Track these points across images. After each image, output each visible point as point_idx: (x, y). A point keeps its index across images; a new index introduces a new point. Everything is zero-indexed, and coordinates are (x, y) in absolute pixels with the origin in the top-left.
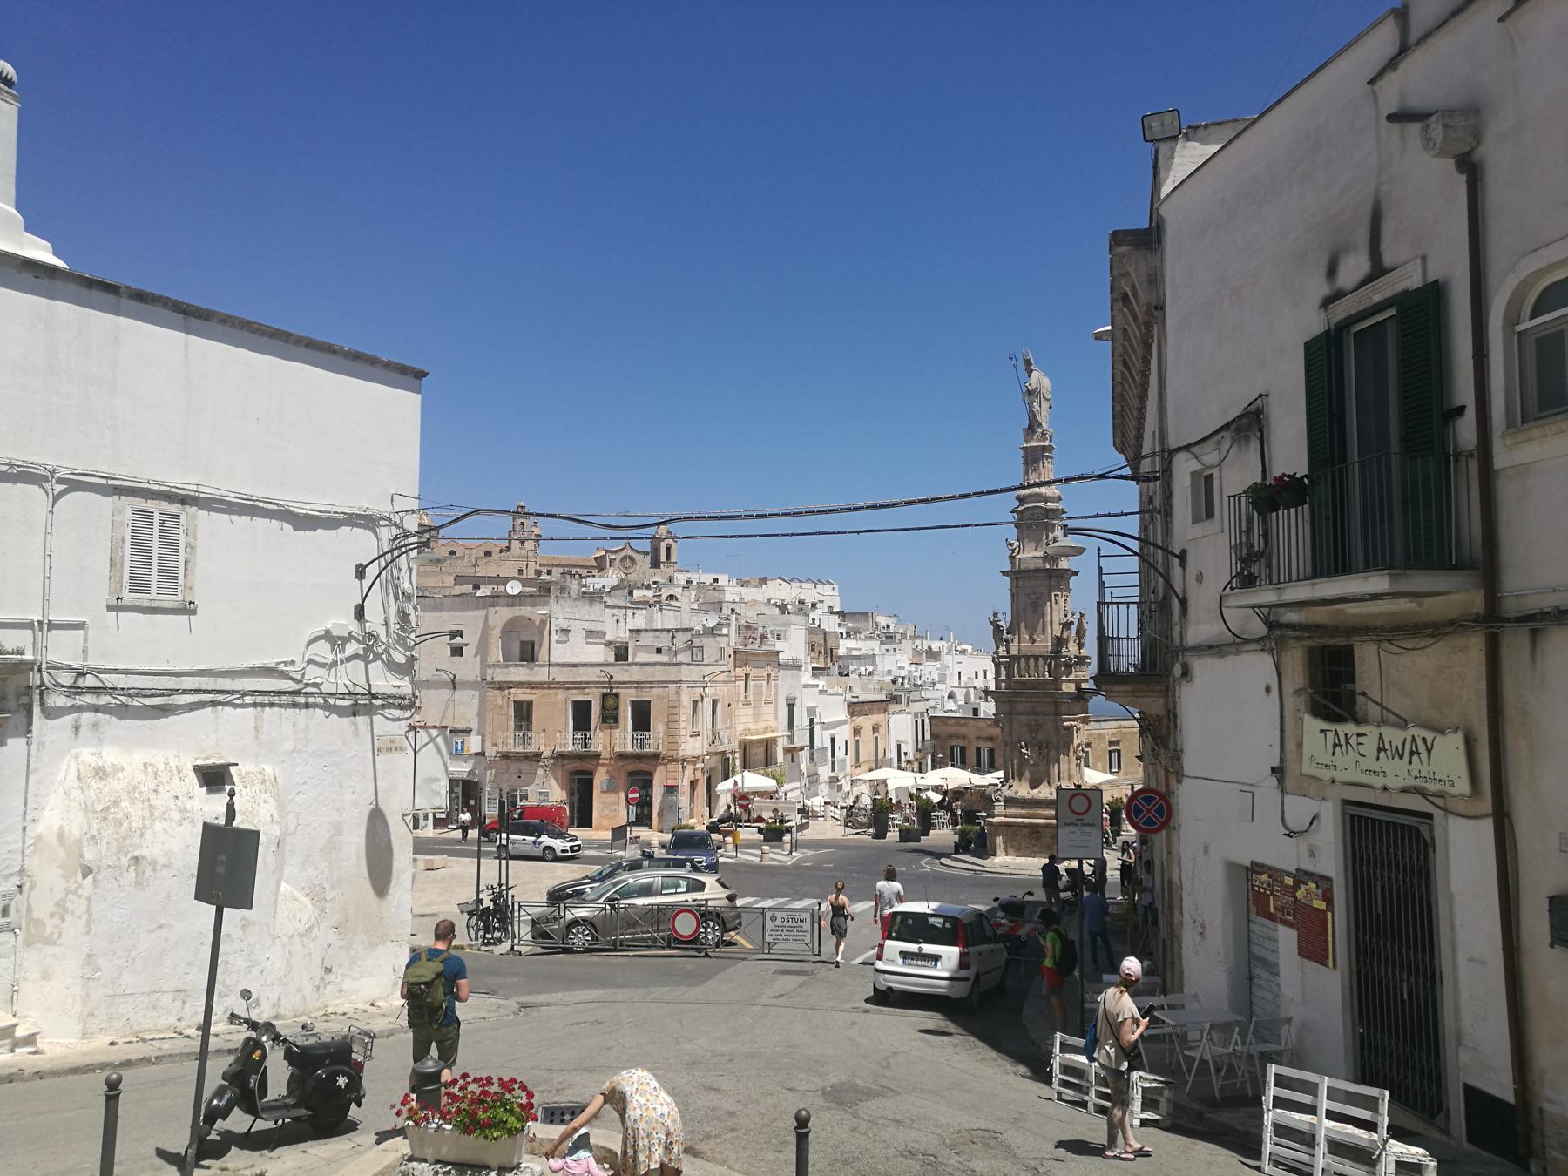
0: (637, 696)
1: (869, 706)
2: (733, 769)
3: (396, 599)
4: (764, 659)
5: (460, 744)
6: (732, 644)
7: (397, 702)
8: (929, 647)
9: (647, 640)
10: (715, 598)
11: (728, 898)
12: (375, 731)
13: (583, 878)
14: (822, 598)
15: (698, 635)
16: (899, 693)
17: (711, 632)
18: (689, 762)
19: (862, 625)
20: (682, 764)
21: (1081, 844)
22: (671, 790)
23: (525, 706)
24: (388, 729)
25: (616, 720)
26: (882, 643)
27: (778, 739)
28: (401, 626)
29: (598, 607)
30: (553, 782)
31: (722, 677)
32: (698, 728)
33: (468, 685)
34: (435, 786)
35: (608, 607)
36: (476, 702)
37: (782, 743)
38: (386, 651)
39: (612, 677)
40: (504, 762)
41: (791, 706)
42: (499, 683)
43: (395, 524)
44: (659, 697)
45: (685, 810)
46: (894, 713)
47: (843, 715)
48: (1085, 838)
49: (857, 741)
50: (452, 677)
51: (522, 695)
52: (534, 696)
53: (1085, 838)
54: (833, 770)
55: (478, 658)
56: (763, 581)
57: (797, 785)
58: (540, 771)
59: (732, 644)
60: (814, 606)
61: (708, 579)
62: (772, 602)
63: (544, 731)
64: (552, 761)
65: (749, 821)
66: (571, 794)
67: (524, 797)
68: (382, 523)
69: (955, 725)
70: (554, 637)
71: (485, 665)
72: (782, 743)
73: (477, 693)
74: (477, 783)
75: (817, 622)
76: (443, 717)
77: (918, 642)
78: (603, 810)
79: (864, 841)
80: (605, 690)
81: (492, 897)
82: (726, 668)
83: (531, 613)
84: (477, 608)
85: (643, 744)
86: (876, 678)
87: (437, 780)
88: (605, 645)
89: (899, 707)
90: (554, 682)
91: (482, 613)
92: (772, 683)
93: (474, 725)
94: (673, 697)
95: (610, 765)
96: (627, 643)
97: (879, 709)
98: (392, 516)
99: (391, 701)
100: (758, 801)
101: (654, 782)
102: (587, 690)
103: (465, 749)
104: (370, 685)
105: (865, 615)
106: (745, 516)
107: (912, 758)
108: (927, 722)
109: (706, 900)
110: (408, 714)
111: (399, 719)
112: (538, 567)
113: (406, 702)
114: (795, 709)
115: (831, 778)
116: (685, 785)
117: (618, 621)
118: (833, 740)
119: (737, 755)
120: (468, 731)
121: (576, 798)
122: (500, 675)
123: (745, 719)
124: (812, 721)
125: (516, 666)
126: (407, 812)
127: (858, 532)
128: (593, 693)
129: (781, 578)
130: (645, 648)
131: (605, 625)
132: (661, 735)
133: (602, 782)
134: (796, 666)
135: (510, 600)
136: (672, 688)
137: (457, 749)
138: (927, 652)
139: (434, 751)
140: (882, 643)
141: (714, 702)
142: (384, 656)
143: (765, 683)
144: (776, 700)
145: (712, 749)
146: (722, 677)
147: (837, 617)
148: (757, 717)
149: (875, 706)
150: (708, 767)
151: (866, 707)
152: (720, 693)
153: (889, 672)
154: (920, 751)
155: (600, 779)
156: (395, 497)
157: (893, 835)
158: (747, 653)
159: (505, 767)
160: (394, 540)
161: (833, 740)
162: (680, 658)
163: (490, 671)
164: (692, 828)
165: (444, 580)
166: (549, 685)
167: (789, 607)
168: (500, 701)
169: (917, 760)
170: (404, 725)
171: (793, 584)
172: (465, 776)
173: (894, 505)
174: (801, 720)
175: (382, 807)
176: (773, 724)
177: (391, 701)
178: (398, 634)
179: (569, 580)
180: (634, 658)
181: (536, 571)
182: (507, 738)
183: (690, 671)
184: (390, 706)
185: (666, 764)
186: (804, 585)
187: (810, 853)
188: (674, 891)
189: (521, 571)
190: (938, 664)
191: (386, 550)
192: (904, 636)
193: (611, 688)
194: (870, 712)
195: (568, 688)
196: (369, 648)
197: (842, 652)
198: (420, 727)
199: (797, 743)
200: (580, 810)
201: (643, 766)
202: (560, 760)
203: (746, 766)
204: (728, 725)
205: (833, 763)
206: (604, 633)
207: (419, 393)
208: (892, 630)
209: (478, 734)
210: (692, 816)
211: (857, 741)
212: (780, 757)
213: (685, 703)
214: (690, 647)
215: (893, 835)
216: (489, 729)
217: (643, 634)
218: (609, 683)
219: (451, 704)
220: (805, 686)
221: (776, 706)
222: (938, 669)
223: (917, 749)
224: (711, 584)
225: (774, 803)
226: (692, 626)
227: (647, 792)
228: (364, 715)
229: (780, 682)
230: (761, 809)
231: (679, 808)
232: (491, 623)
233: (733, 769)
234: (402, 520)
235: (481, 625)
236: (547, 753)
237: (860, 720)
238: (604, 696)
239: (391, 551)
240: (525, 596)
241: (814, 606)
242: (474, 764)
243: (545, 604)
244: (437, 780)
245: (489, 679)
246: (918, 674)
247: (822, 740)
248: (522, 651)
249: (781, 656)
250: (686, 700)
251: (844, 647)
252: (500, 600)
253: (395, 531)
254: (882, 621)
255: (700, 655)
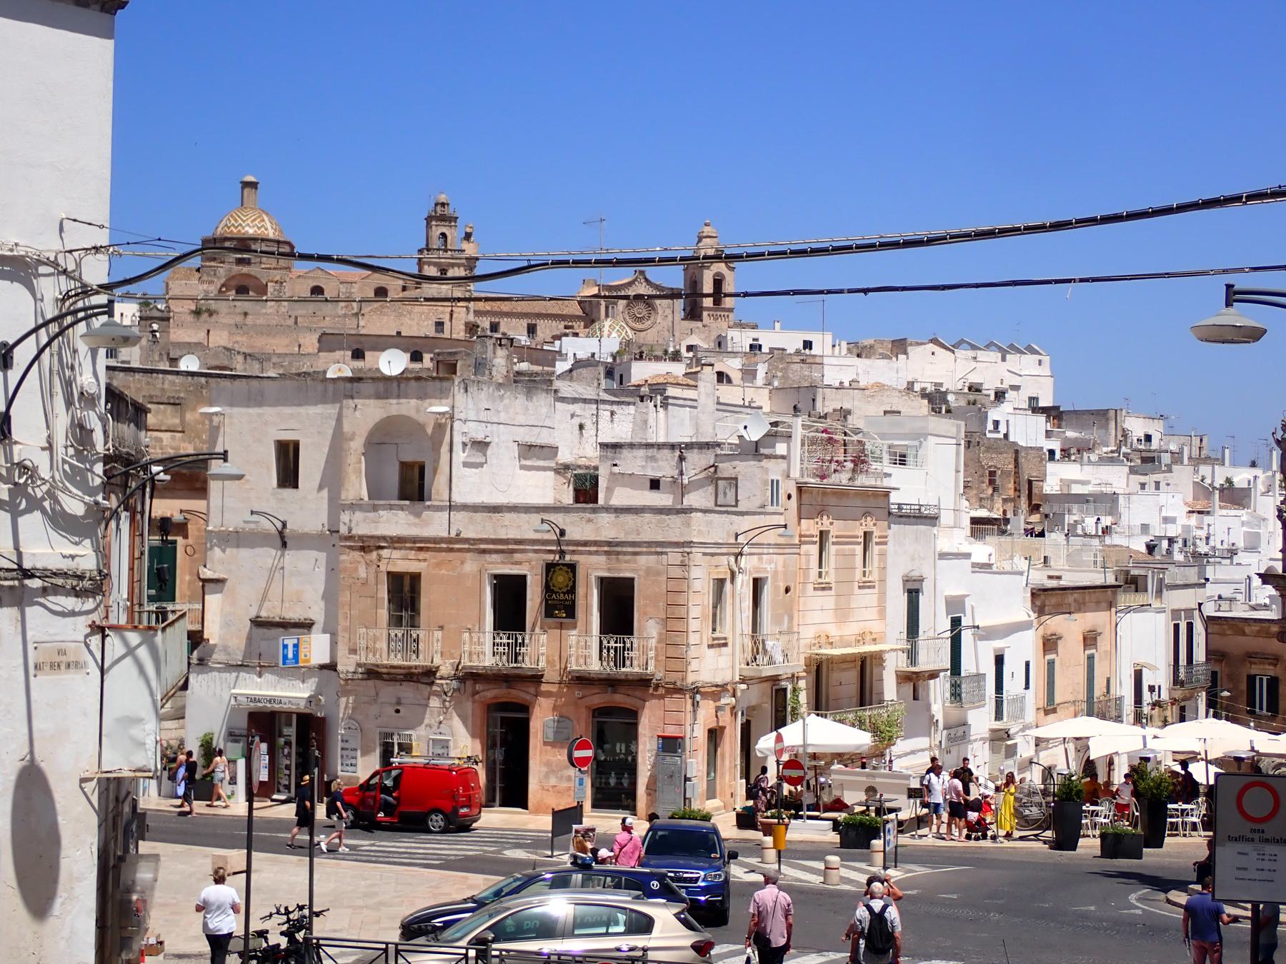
0: (609, 570)
1: (1076, 595)
2: (794, 709)
3: (69, 403)
4: (858, 503)
5: (290, 649)
6: (796, 473)
7: (71, 582)
8: (1229, 481)
9: (633, 463)
10: (803, 378)
11: (695, 947)
12: (29, 634)
13: (465, 901)
14: (1016, 381)
15: (729, 457)
16: (1142, 572)
17: (754, 451)
18: (705, 695)
19: (1093, 434)
20: (693, 698)
21: (1257, 875)
22: (671, 745)
23: (407, 581)
24: (51, 631)
25: (571, 611)
26: (1133, 471)
27: (886, 656)
28: (76, 450)
29: (542, 402)
30: (457, 722)
31: (771, 537)
32: (725, 631)
33: (307, 541)
34: (135, 732)
35: (563, 400)
36: (321, 573)
37: (894, 663)
38: (51, 494)
39: (562, 533)
40: (370, 683)
41: (913, 595)
42: (361, 538)
43: (65, 272)
44: (649, 571)
45: (698, 784)
46: (1128, 610)
47: (1022, 610)
48: (1267, 865)
49: (1051, 664)
50: (279, 525)
51: (402, 562)
52: (423, 565)
53: (1267, 865)
54: (999, 715)
55: (325, 493)
56: (900, 347)
57: (922, 742)
58: (435, 703)
59: (796, 473)
60: (1000, 395)
61: (792, 341)
62: (917, 387)
63: (441, 628)
64: (455, 684)
65: (815, 807)
66: (489, 746)
67: (406, 748)
68: (42, 270)
69: (1258, 634)
70: (460, 456)
71: (336, 506)
72: (894, 663)
73: (322, 556)
74: (323, 720)
75: (1002, 428)
76: (264, 598)
77: (1205, 470)
78: (547, 776)
79: (1032, 853)
80: (550, 557)
81: (285, 927)
82: (780, 520)
83: (418, 411)
84: (323, 400)
85: (620, 660)
86: (1115, 539)
87: (139, 721)
88: (557, 471)
89: (1140, 599)
90: (458, 540)
91: (331, 410)
92: (875, 550)
93: (317, 613)
94: (676, 572)
95: (558, 695)
96: (596, 468)
97: (1098, 603)
98: (61, 261)
99: (60, 581)
100: (839, 772)
101: (641, 729)
102: (517, 556)
103: (302, 656)
104: (20, 555)
105: (1101, 416)
106: (662, 260)
107: (1165, 696)
108: (1199, 629)
109: (645, 950)
110: (90, 604)
111: (73, 614)
112: (471, 318)
113: (87, 584)
114: (923, 600)
115: (993, 731)
116: (697, 736)
117: (581, 427)
118: (999, 660)
119: (802, 684)
120: (307, 626)
121: (499, 755)
122: (363, 525)
123: (817, 617)
124: (956, 622)
125: (391, 507)
126: (87, 775)
127: (866, 291)
128: (529, 561)
129: (935, 341)
130: (629, 480)
131: (556, 433)
132: (653, 643)
133: (545, 725)
134: (924, 518)
135: (381, 386)
136: (674, 556)
137: (285, 657)
138: (1222, 490)
139: (134, 671)
140: (1133, 471)
141: (757, 584)
142: (46, 504)
143: (859, 549)
144: (883, 581)
145: (750, 671)
146: (771, 537)
147: (1042, 418)
148: (842, 613)
149: (1088, 596)
150: (744, 704)
151: (1071, 598)
152: (770, 567)
153: (1145, 528)
154: (1182, 684)
155: (542, 720)
156: (67, 224)
157: (1089, 844)
158: (824, 492)
159: (373, 693)
160: (63, 300)
161: (999, 660)
162: (692, 499)
163: (345, 517)
164: (707, 818)
165: (302, 341)
166: (451, 545)
167: (951, 398)
168: (362, 572)
169: (1174, 701)
170: (82, 624)
171: (960, 353)
172: (302, 707)
173: (931, 241)
174: (934, 621)
175: (43, 765)
176: (876, 627)
177: (60, 581)
178: (71, 465)
179: (490, 348)
180: (608, 498)
181: (467, 324)
182: (375, 639)
183: (710, 523)
184: (56, 590)
185: (662, 697)
186: (981, 355)
187: (920, 870)
188: (603, 930)
189: (440, 325)
190: (1244, 514)
191: (49, 316)
192: (1177, 458)
193: (562, 553)
194: (1081, 607)
195: (484, 551)
196: (18, 490)
197: (1051, 486)
198: (110, 628)
199: (924, 664)
200: (505, 775)
201: (620, 699)
202: (469, 683)
203: (820, 705)
204: (785, 627)
205: (999, 704)
206: (554, 450)
207: (110, 36)
208: (1155, 444)
209: (324, 631)
210: (711, 794)
211: (1051, 664)
212: (890, 689)
213: (697, 585)
214: (713, 477)
215: (1089, 844)
216: (343, 623)
217: (626, 452)
218: (559, 543)
219: (278, 575)
220: (943, 556)
221: (882, 595)
222: (1243, 524)
223: (1176, 681)
224: (798, 352)
225: (868, 775)
226: (720, 438)
227: (628, 747)
228: (11, 605)
229: (890, 548)
230: (842, 786)
231: (687, 779)
232: (347, 427)
233: (794, 709)
234: (78, 265)
235: (330, 432)
236: (446, 669)
237: (1057, 623)
238: (550, 567)
239: (61, 317)
240: (408, 379)
241: (1000, 395)
242: (319, 685)
243: (443, 394)
244: (139, 721)
245: (343, 530)
246: (1203, 534)
247: (977, 659)
248: (404, 481)
249: (895, 498)
250: (701, 577)
251: (1056, 477)
252: (361, 385)
253: (65, 284)
254: (1136, 427)
255: (731, 494)
